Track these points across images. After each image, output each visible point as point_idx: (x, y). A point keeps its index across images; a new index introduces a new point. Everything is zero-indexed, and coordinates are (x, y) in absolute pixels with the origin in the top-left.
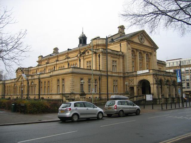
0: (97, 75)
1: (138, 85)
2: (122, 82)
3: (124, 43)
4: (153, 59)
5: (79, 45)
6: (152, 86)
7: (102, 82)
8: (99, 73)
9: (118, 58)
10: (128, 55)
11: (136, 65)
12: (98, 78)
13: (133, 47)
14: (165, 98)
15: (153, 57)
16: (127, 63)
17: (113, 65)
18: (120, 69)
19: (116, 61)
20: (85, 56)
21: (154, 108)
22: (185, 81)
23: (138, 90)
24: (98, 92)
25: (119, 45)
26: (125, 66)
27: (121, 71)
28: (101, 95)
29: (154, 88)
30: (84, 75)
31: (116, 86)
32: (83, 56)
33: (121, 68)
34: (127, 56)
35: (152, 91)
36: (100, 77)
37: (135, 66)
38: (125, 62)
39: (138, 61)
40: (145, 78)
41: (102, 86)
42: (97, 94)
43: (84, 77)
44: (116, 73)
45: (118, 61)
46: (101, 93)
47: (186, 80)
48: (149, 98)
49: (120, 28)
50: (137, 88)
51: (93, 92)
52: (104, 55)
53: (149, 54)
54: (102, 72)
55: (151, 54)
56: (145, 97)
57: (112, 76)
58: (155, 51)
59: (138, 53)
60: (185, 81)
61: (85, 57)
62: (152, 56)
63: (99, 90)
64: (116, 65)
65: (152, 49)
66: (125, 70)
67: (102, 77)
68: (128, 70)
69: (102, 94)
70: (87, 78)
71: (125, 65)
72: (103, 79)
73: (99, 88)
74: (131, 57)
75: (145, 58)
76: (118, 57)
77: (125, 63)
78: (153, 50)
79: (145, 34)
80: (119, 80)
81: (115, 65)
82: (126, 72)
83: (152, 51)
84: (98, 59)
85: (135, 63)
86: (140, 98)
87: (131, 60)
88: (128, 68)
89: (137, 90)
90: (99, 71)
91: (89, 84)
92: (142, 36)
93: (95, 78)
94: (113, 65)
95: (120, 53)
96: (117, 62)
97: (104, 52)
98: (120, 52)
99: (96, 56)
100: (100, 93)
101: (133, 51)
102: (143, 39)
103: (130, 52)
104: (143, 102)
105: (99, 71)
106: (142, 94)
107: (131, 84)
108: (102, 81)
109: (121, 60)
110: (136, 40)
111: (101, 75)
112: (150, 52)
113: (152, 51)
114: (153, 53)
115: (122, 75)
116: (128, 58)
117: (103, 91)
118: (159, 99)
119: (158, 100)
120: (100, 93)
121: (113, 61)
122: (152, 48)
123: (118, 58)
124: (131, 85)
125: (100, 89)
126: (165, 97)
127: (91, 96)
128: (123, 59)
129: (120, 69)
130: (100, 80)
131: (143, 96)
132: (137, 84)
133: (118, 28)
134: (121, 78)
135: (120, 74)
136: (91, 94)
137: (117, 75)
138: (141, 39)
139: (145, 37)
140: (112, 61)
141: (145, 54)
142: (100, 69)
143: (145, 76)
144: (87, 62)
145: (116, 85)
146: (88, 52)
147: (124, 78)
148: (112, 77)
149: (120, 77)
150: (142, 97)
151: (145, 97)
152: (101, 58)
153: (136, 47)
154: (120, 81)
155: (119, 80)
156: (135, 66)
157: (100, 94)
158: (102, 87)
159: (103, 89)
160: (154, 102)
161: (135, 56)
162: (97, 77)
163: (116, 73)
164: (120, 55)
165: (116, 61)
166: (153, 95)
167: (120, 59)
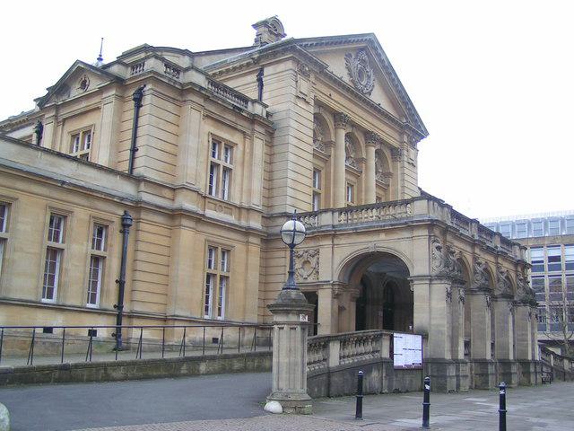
0: (108, 198)
1: (342, 285)
2: (255, 259)
3: (281, 67)
4: (406, 178)
5: (475, 221)
6: (419, 290)
7: (141, 246)
8: (126, 189)
9: (244, 133)
10: (295, 125)
11: (327, 188)
12: (117, 221)
13: (324, 99)
14: (476, 361)
15: (406, 171)
16: (290, 166)
17: (212, 271)
18: (250, 192)
19: (229, 147)
20: (65, 104)
21: (365, 411)
22: (560, 269)
23: (341, 309)
24: (110, 303)
25: (253, 78)
26: (277, 183)
27: (256, 201)
28: (125, 322)
29: (430, 304)
30: (20, 185)
31: (222, 278)
32: (57, 107)
33: (258, 185)
34: (292, 132)
35: (419, 318)
36: (132, 214)
37: (322, 192)
38: (277, 158)
39: (343, 175)
40: (382, 243)
41: (140, 266)
42: (101, 312)
43: (23, 198)
44: (229, 207)
45: (240, 146)
46: (126, 308)
47: (564, 267)
48: (407, 350)
49: (262, 29)
50: (336, 296)
51: (75, 297)
52: (166, 98)
53: (387, 153)
54: (142, 184)
55: (396, 153)
56: (386, 343)
57: (199, 219)
58: (413, 145)
59: (342, 133)
60: (560, 269)
61: (65, 113)
62: (399, 165)
63: (114, 287)
64: (228, 165)
65: (401, 134)
66: (277, 201)
67: (143, 215)
68: (289, 201)
69: (131, 316)
70: (44, 202)
71: (277, 175)
72: (143, 226)
73: (115, 275)
74: (310, 149)
75: (372, 161)
76: (243, 125)
77: (277, 166)
78: (405, 139)
79: (379, 55)
80: (239, 249)
81: (222, 163)
82: (277, 210)
83: (402, 142)
84: (130, 115)
85: (328, 179)
86: (361, 349)
87: (308, 164)
88: (290, 192)
89: (336, 307)
90: (130, 176)
91: (53, 244)
92: (364, 61)
93: (95, 213)
94: (209, 276)
95: (258, 110)
96: (238, 152)
97: (170, 80)
98: (254, 102)
99: (121, 98)
100: (119, 306)
101: (325, 118)
102: (369, 77)
103: (308, 112)
104: (375, 374)
105: (139, 180)
106: (356, 330)
107: (304, 275)
108: (137, 241)
109: (259, 146)
110: (338, 67)
111: (138, 206)
112: (396, 144)
113: (402, 142)
114: (405, 152)
115: (256, 223)
116: (292, 140)
117: (138, 296)
118: (456, 362)
119: (451, 371)
120: (119, 306)
121: (216, 142)
122: (402, 129)
123: (244, 133)
124: (301, 280)
125: (121, 283)
126: (476, 351)
127: (57, 320)
128: (270, 144)
129: (246, 188)
130: (125, 227)
131: (377, 339)
132: (336, 279)
133: (255, 26)
134: (252, 239)
135: (248, 220)
136: (60, 308)
137: (232, 219)
138: (360, 74)
139: (376, 71)
140: (206, 141)
141: (373, 149)
142: (136, 172)
143: (382, 236)
144: (75, 136)
145: (219, 273)
146: (84, 85)
147: (269, 240)
148: (201, 228)
149: (248, 232)
150: (369, 347)
151: (386, 343)
152: (145, 110)
153: (339, 103)
154: (244, 255)
155: (239, 249)
156: (322, 192)
157: (119, 318)
158: (139, 276)
159: (139, 286)
160: (430, 379)
161: (329, 144)
162: (114, 215)
163: (229, 207)
164: (253, 119)
165: (229, 147)
166: (425, 337)
167: (252, 141)
